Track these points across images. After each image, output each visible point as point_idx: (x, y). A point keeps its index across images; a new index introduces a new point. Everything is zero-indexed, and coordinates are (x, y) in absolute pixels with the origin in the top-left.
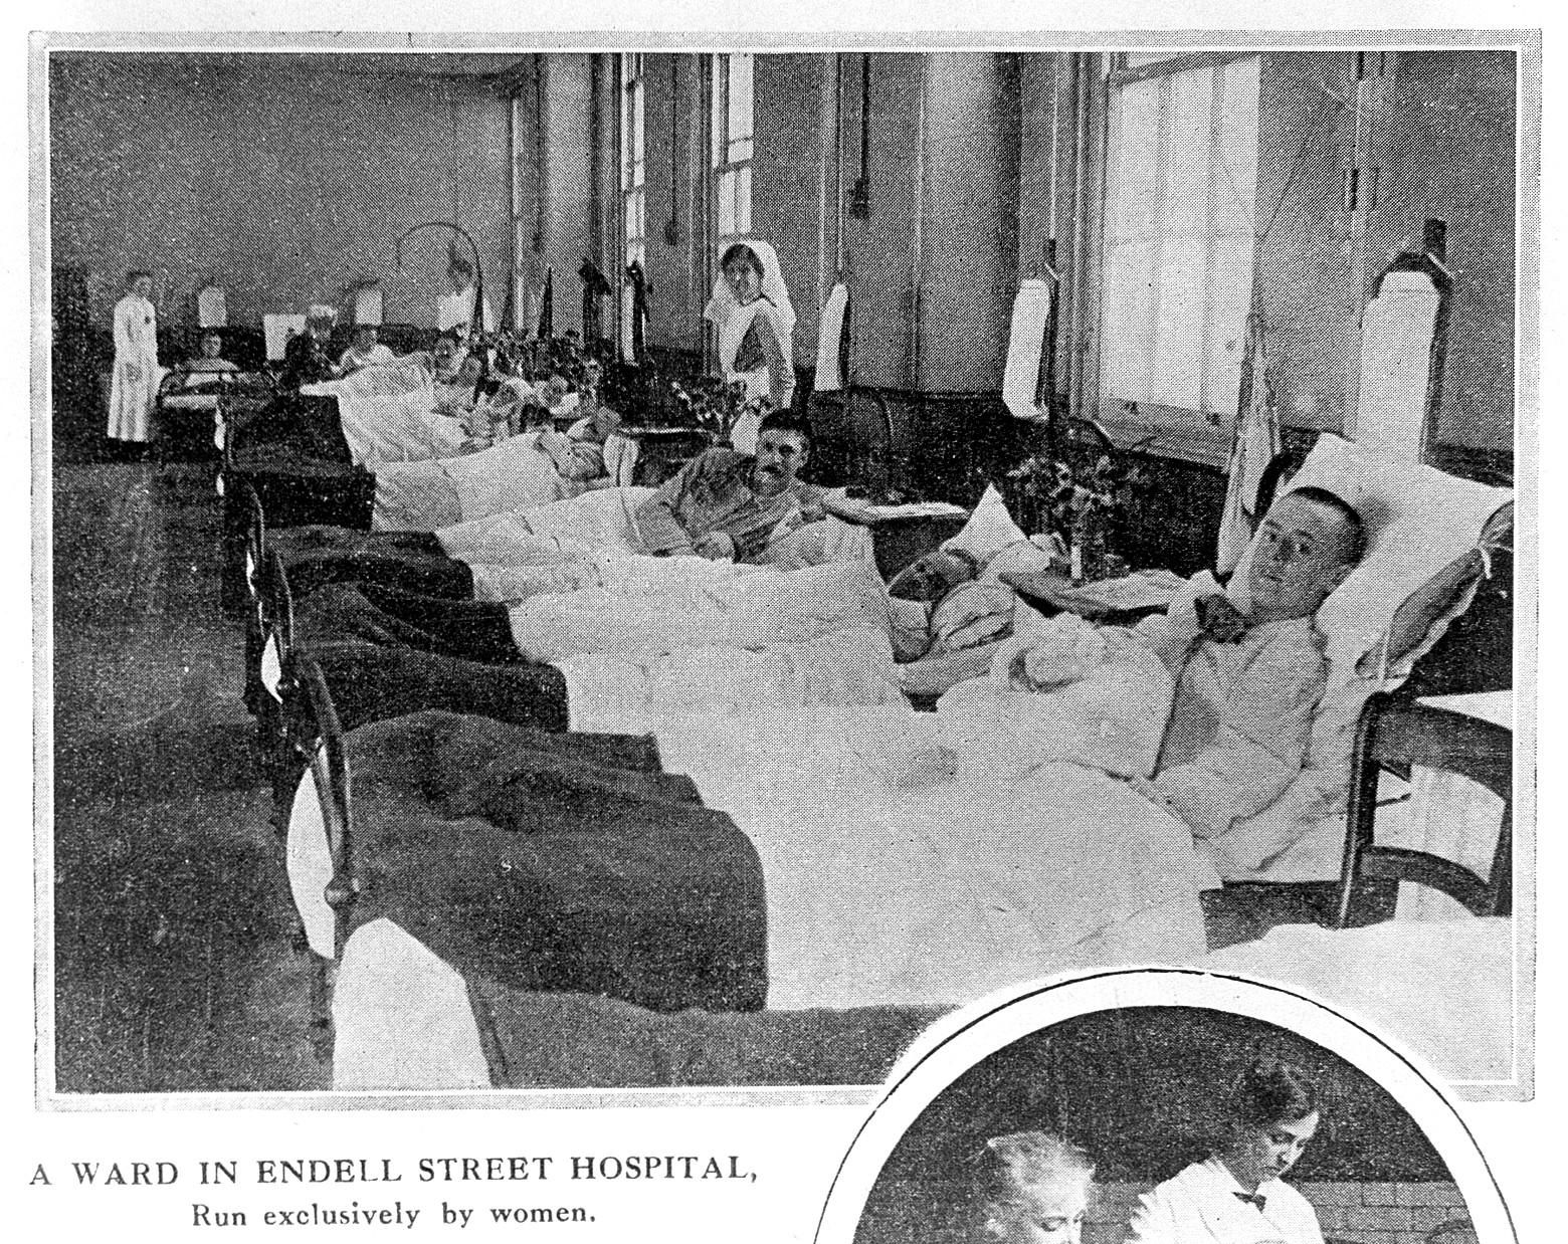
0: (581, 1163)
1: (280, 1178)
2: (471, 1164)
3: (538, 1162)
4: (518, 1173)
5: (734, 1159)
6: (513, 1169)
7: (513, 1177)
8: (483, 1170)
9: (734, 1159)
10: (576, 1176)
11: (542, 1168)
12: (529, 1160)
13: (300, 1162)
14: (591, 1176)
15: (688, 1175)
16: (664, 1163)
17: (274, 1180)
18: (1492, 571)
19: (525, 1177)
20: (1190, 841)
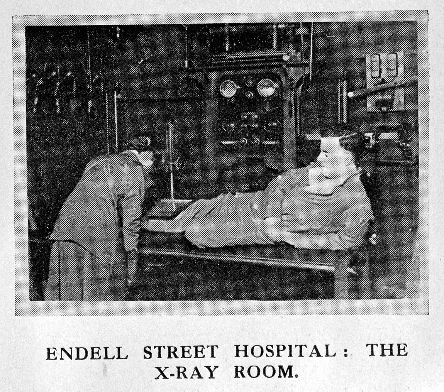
0: (240, 348)
1: (59, 357)
2: (172, 350)
3: (298, 347)
4: (199, 354)
5: (327, 346)
6: (196, 352)
7: (196, 356)
8: (179, 353)
9: (327, 346)
10: (237, 355)
11: (301, 352)
12: (205, 347)
13: (71, 348)
14: (246, 356)
15: (301, 355)
16: (288, 348)
17: (56, 359)
18: (276, 141)
19: (204, 357)
20: (278, 227)
